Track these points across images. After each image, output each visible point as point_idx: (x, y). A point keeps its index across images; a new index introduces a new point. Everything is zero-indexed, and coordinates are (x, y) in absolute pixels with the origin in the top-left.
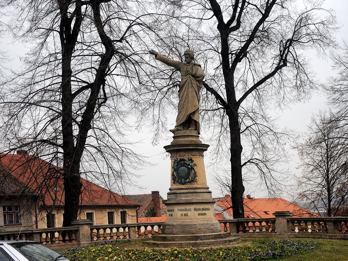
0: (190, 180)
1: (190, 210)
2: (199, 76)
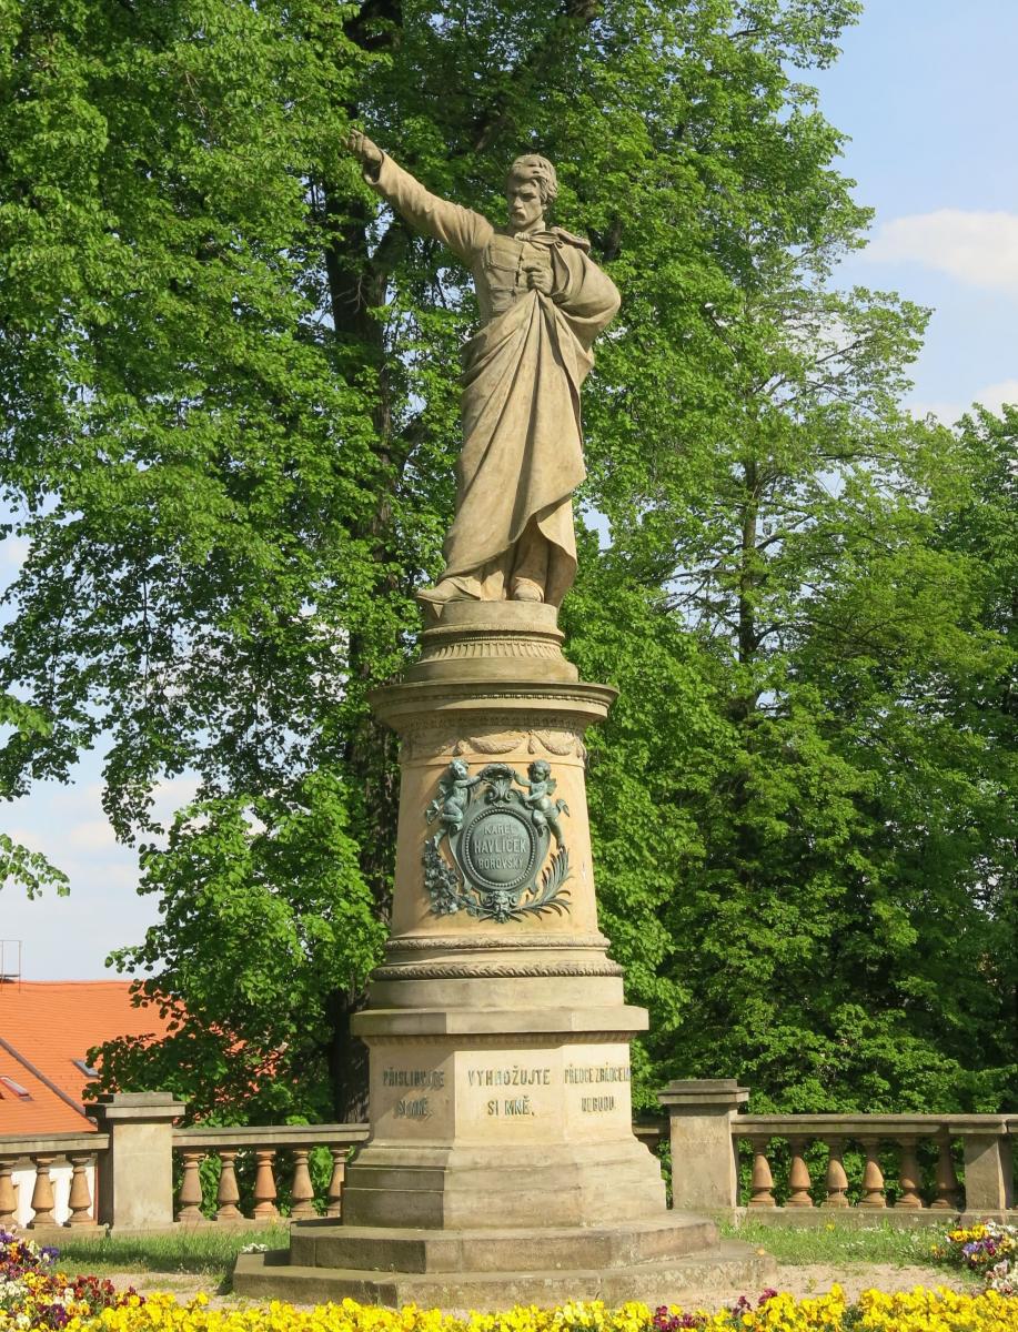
0: (539, 895)
1: (541, 1076)
2: (594, 303)
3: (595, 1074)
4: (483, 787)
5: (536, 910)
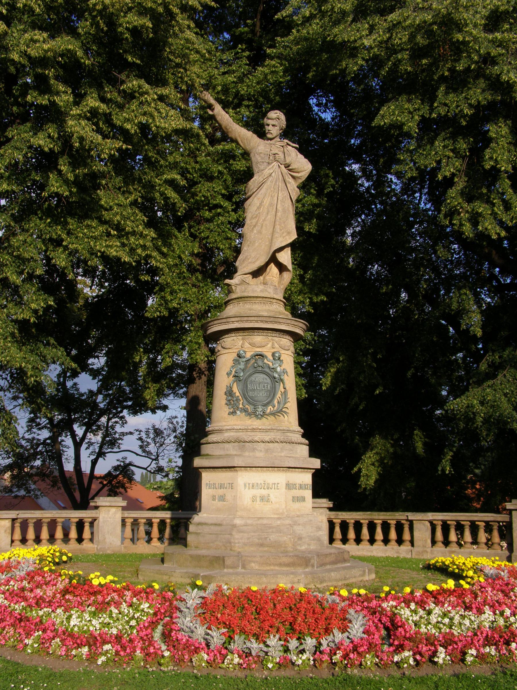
0: (275, 408)
3: (297, 485)
4: (253, 361)
5: (273, 414)
